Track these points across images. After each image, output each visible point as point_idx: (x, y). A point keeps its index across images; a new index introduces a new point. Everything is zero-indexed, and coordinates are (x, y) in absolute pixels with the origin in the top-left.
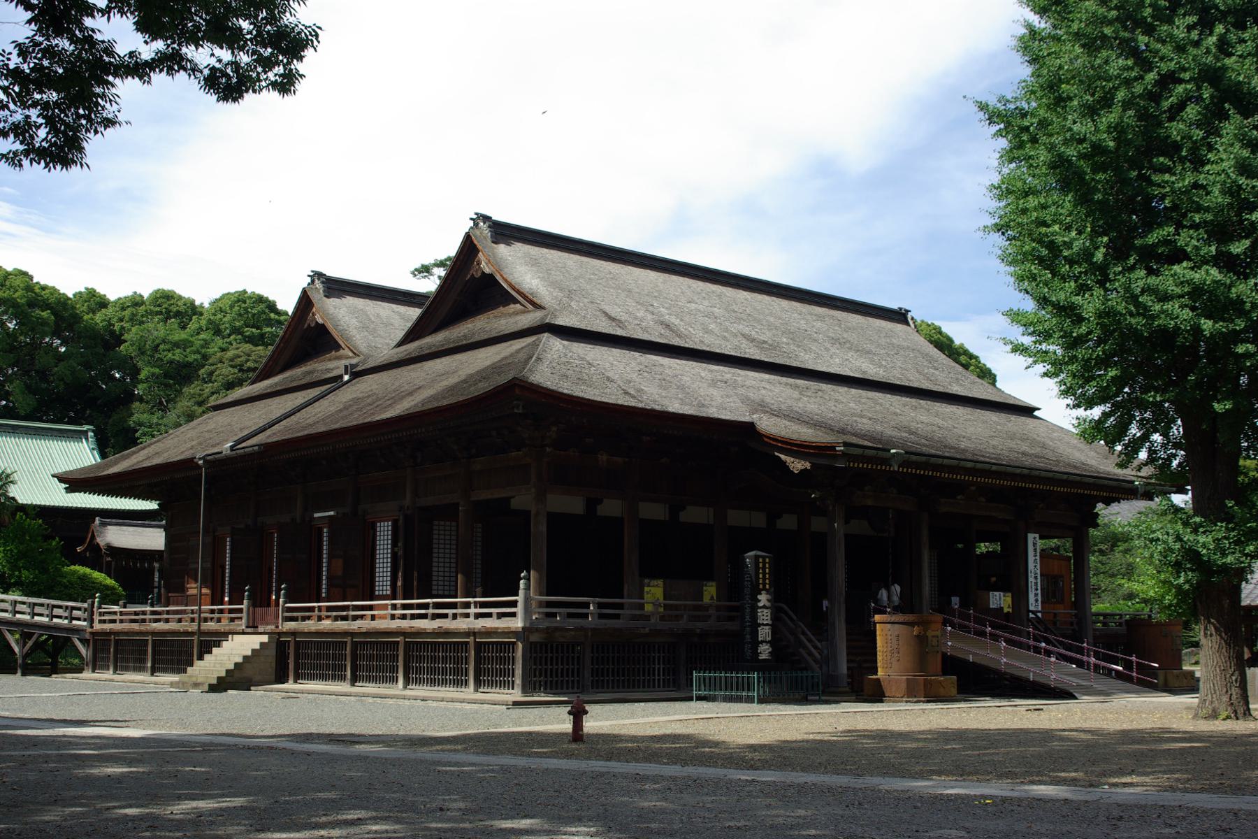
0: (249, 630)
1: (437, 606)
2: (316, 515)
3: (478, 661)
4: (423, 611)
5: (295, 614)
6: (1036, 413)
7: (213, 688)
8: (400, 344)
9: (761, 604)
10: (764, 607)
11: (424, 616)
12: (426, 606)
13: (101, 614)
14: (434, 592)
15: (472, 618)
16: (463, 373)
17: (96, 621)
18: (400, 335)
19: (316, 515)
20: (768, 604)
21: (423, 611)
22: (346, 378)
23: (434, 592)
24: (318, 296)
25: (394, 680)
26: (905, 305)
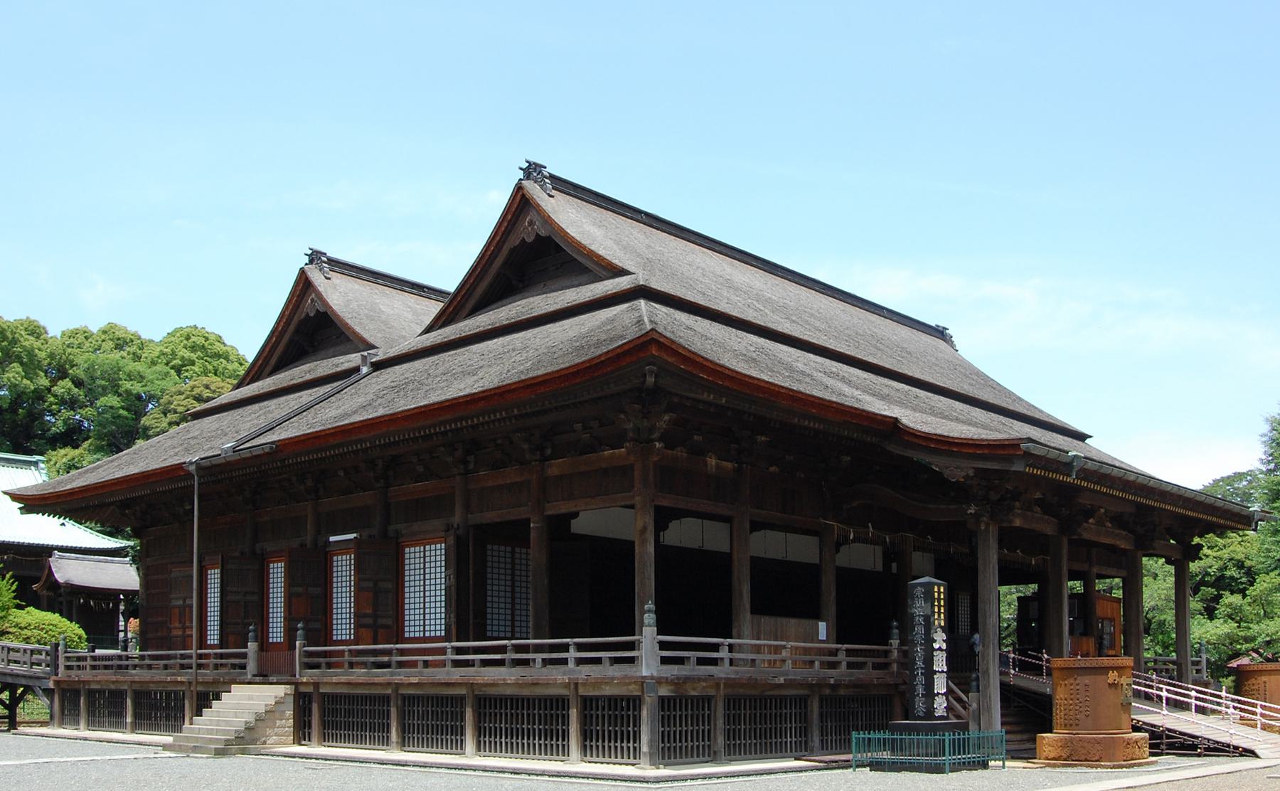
0: (257, 679)
1: (518, 649)
2: (332, 539)
3: (585, 721)
4: (498, 657)
5: (316, 660)
6: (1088, 441)
7: (220, 753)
8: (428, 330)
9: (936, 646)
10: (940, 649)
11: (500, 663)
12: (502, 650)
13: (68, 659)
14: (489, 634)
15: (571, 665)
16: (584, 329)
17: (61, 669)
18: (428, 320)
19: (332, 539)
20: (944, 646)
21: (498, 657)
22: (365, 370)
23: (489, 634)
24: (316, 277)
25: (565, 751)
26: (942, 324)
